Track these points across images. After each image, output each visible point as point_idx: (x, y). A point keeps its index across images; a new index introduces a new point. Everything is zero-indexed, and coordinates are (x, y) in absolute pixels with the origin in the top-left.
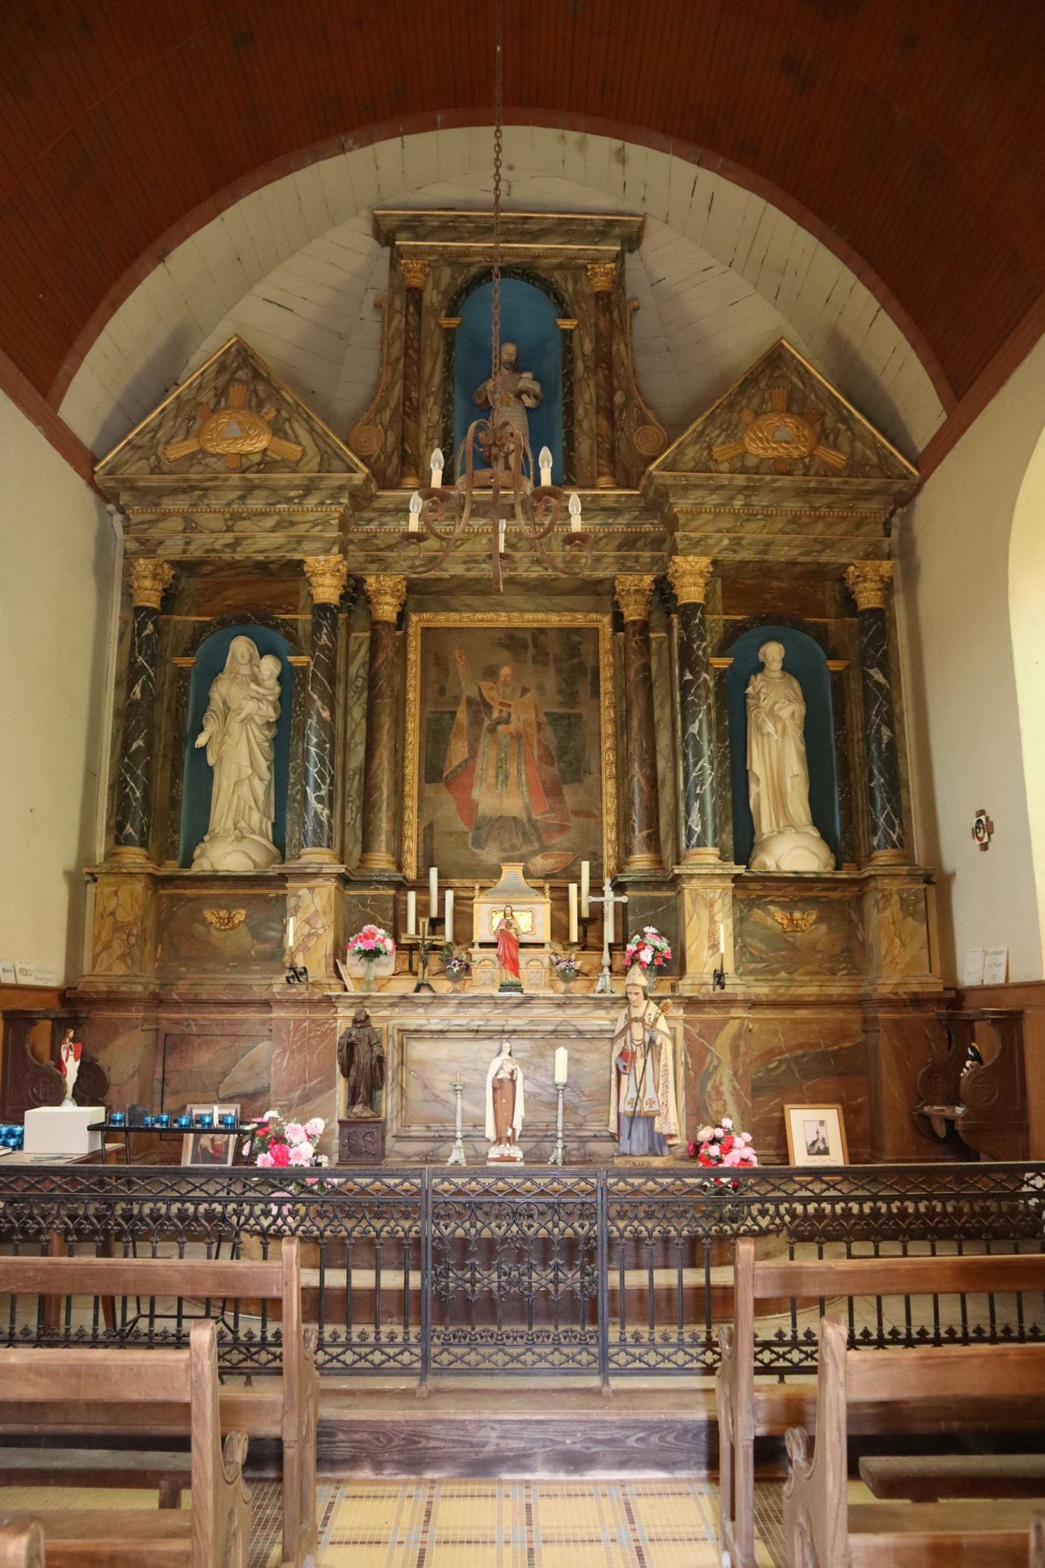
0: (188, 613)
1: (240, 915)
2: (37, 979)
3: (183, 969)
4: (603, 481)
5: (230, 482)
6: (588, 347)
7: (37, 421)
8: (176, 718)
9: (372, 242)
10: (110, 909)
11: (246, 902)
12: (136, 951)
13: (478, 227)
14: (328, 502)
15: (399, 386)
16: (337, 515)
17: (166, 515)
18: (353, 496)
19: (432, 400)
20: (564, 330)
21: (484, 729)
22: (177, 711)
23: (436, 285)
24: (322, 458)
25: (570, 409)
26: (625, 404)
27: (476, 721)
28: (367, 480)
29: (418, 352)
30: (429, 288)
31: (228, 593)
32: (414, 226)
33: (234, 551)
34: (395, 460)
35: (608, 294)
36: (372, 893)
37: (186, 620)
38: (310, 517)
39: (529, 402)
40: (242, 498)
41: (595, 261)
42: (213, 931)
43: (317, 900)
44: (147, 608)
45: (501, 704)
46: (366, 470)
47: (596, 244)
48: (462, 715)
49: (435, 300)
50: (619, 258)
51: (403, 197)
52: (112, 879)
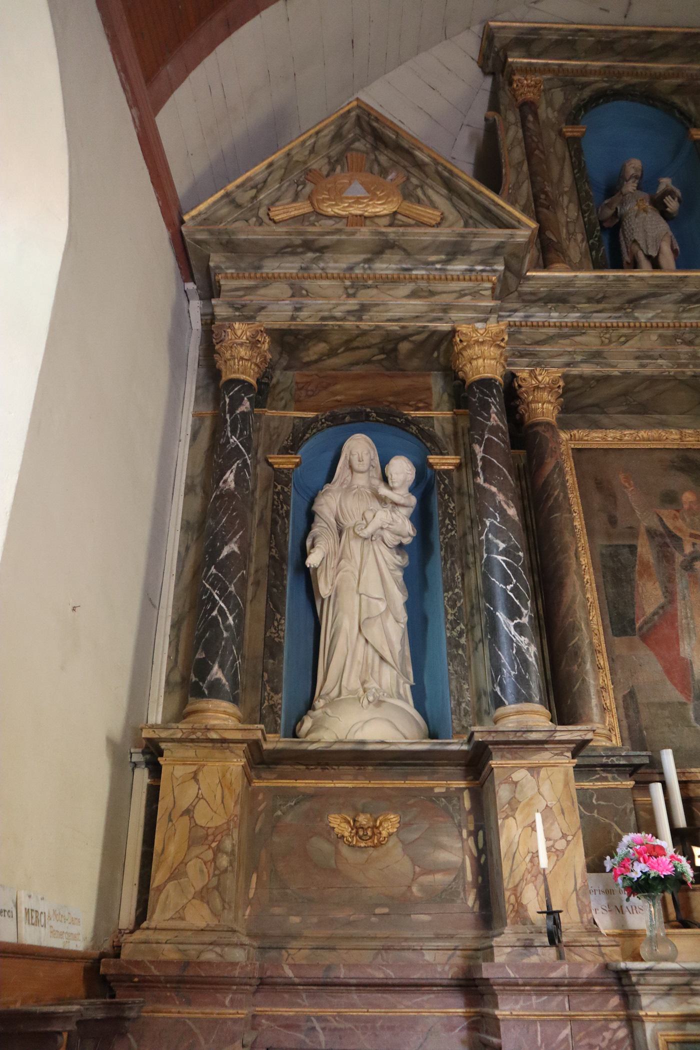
0: (285, 408)
1: (390, 823)
2: (54, 933)
3: (295, 920)
5: (358, 237)
7: (134, 102)
8: (273, 532)
9: (475, 69)
10: (184, 804)
11: (400, 801)
12: (229, 881)
13: (599, 42)
16: (489, 285)
17: (268, 280)
21: (677, 566)
22: (274, 522)
23: (550, 104)
27: (665, 557)
31: (338, 387)
32: (527, 41)
33: (360, 319)
36: (599, 785)
37: (283, 415)
38: (455, 286)
40: (368, 261)
42: (345, 850)
43: (546, 788)
44: (244, 381)
45: (692, 535)
46: (534, 225)
48: (646, 550)
49: (551, 116)
52: (189, 752)
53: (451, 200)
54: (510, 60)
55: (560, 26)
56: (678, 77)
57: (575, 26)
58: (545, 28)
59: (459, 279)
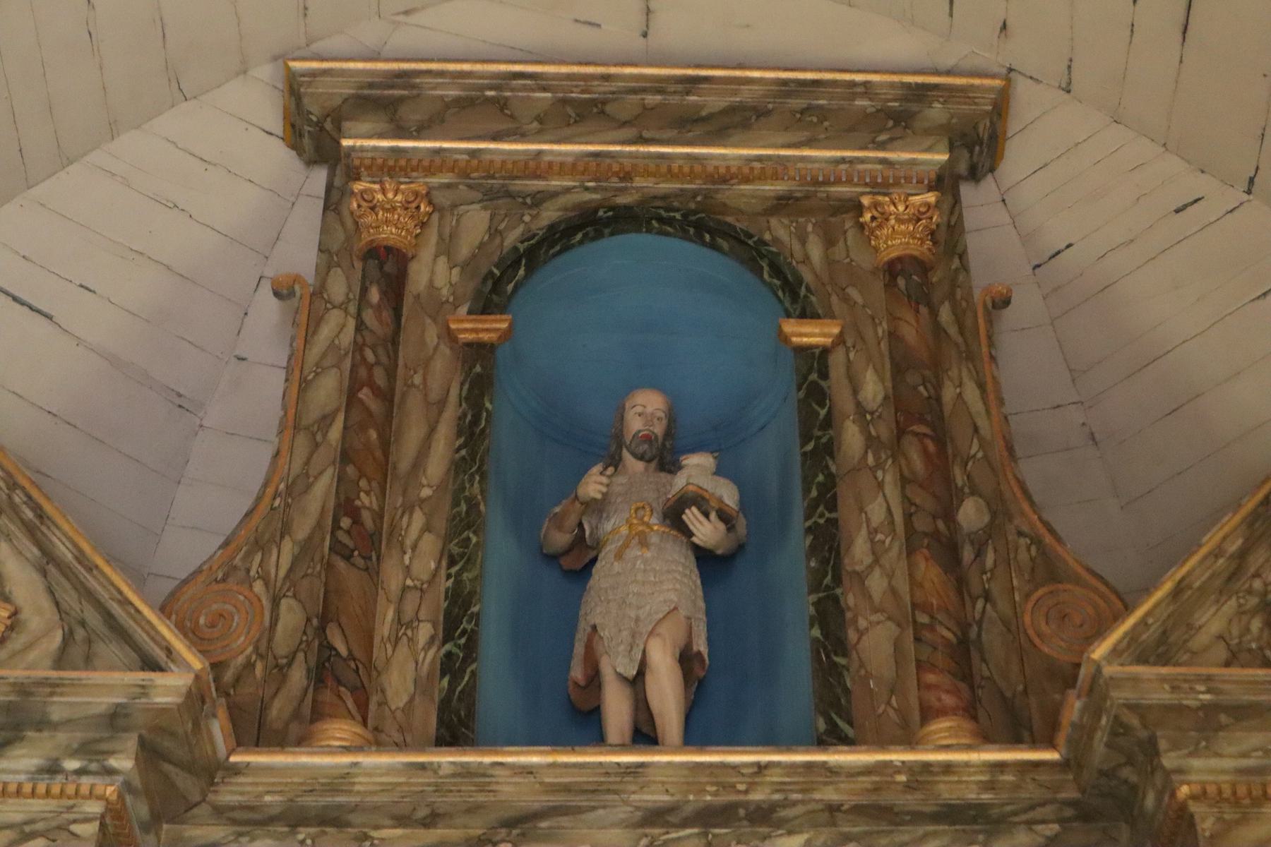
4: (940, 727)
6: (873, 389)
9: (279, 157)
13: (565, 102)
14: (72, 764)
15: (323, 488)
16: (95, 808)
18: (150, 753)
19: (418, 519)
20: (802, 350)
23: (447, 247)
24: (68, 639)
25: (827, 544)
26: (991, 532)
28: (196, 699)
29: (387, 397)
30: (427, 253)
32: (388, 99)
34: (298, 676)
35: (922, 267)
39: (706, 531)
41: (880, 187)
46: (197, 663)
47: (882, 146)
49: (440, 281)
50: (946, 182)
51: (370, 33)
53: (44, 573)
54: (346, 143)
55: (466, 67)
56: (776, 177)
57: (503, 68)
58: (429, 73)
59: (19, 793)
